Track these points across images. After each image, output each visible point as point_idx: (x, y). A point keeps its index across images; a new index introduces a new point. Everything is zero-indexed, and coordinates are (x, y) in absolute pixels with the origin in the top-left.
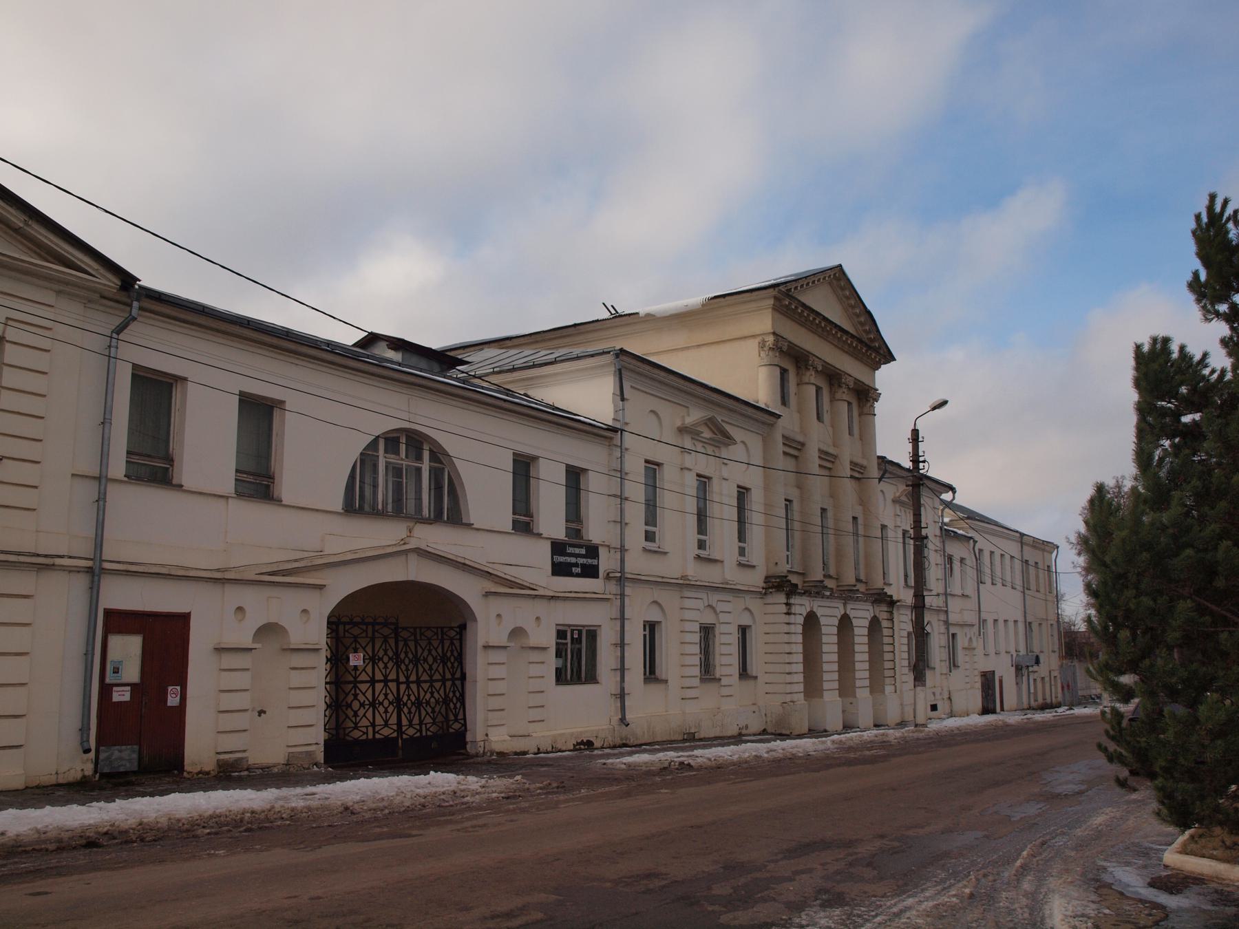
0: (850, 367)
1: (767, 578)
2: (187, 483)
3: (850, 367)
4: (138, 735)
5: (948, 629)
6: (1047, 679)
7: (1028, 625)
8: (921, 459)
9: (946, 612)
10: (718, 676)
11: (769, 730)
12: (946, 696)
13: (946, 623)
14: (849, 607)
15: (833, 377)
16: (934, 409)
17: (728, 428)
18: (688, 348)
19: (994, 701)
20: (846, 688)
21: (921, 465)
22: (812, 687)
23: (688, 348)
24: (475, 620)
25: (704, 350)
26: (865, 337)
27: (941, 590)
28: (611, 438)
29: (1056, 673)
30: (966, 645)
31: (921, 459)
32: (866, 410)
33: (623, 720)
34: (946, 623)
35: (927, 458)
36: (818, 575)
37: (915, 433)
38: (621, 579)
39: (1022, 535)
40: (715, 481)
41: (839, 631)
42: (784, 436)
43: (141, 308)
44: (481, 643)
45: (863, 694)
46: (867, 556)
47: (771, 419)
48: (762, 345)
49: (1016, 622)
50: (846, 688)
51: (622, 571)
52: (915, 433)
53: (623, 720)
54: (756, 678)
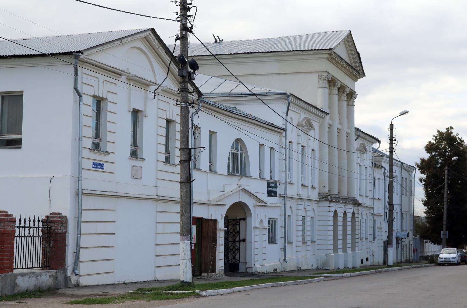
0: (342, 78)
1: (319, 194)
2: (219, 172)
3: (342, 78)
4: (362, 262)
5: (373, 217)
6: (408, 246)
7: (402, 214)
8: (394, 139)
9: (373, 208)
10: (306, 241)
11: (319, 268)
12: (371, 254)
13: (373, 214)
14: (347, 207)
15: (342, 89)
16: (401, 115)
17: (312, 122)
18: (279, 74)
19: (14, 246)
20: (345, 250)
21: (394, 142)
22: (335, 249)
23: (279, 74)
24: (251, 216)
25: (288, 76)
26: (354, 65)
27: (371, 197)
28: (281, 133)
29: (411, 243)
30: (379, 227)
31: (394, 139)
32: (350, 103)
33: (285, 260)
34: (373, 214)
35: (397, 138)
36: (336, 192)
37: (392, 125)
38: (285, 197)
39: (402, 163)
40: (306, 148)
41: (343, 219)
42: (328, 124)
43: (202, 106)
44: (253, 226)
45: (349, 251)
46: (340, 176)
47: (322, 115)
48: (320, 78)
49: (397, 212)
50: (345, 250)
51: (285, 193)
52: (392, 125)
53: (285, 260)
54: (315, 242)
